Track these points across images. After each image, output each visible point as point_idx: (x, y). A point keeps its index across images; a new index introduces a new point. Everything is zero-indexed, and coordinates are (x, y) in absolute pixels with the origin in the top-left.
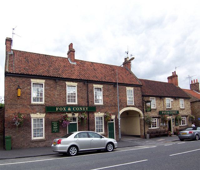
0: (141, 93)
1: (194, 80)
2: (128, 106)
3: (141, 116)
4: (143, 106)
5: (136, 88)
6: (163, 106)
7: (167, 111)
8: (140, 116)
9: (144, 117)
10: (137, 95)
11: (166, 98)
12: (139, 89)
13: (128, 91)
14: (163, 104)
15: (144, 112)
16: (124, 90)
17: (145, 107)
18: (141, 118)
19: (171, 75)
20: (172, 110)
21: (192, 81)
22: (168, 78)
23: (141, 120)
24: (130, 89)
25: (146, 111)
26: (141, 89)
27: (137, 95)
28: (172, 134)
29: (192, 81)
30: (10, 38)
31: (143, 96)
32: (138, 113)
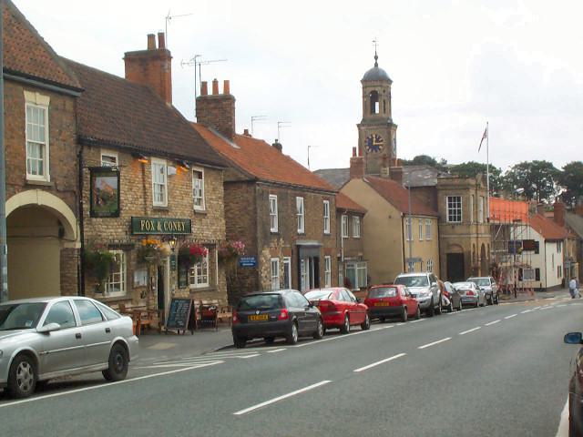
0: (73, 128)
1: (215, 83)
2: (29, 186)
3: (68, 236)
4: (80, 187)
5: (59, 101)
6: (140, 193)
7: (156, 220)
8: (62, 234)
9: (82, 241)
10: (60, 133)
11: (154, 161)
12: (69, 104)
13: (29, 109)
14: (141, 185)
15: (79, 213)
16: (16, 103)
17: (86, 193)
18: (69, 245)
19: (142, 46)
20: (170, 215)
21: (204, 85)
22: (130, 58)
23: (66, 256)
24: (37, 105)
25: (93, 214)
26: (75, 107)
27: (60, 133)
28: (518, 194)
29: (204, 85)
30: (395, 139)
31: (81, 142)
32: (59, 220)
